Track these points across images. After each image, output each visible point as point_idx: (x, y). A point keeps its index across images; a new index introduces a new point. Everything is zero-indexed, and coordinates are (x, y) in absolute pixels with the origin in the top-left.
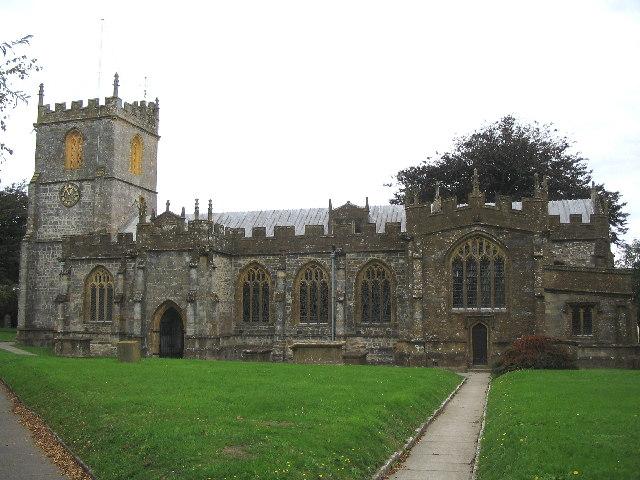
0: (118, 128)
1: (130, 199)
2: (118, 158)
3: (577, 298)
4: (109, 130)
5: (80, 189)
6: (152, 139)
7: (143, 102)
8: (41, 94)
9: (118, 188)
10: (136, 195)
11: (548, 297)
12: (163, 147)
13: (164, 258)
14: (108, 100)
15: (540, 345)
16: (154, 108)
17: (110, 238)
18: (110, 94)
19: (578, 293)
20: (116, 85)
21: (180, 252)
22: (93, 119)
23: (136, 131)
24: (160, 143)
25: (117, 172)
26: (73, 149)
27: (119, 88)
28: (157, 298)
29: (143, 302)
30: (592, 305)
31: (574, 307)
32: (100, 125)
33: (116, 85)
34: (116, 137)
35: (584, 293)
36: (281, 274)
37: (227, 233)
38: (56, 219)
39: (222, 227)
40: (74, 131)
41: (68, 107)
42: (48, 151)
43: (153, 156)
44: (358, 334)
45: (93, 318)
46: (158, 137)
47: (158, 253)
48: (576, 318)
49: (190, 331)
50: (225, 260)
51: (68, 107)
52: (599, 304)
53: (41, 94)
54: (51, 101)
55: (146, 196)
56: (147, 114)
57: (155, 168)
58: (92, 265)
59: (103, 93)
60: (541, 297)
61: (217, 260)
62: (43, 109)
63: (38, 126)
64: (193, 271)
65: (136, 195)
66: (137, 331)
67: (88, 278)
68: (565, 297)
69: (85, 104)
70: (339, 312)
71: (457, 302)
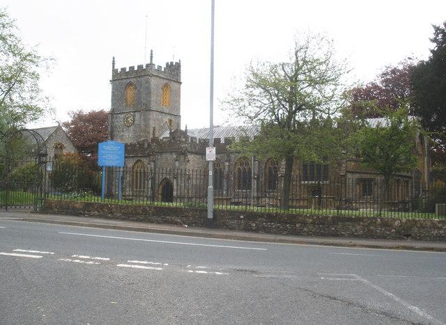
0: (153, 81)
1: (162, 121)
2: (153, 98)
3: (365, 176)
4: (148, 82)
5: (134, 116)
6: (176, 85)
7: (172, 63)
8: (114, 64)
9: (153, 115)
10: (166, 119)
11: (349, 175)
12: (183, 88)
13: (164, 155)
14: (147, 66)
15: (74, 208)
16: (178, 66)
17: (331, 124)
18: (149, 62)
19: (364, 173)
20: (151, 57)
21: (171, 152)
22: (139, 77)
23: (165, 81)
24: (182, 86)
25: (153, 106)
26: (130, 93)
27: (153, 58)
28: (159, 178)
29: (153, 179)
30: (372, 180)
31: (361, 181)
32: (143, 80)
33: (151, 57)
34: (152, 86)
35: (367, 173)
36: (227, 164)
37: (200, 141)
38: (122, 134)
39: (196, 139)
40: (130, 84)
41: (127, 70)
42: (117, 97)
43: (177, 94)
44: (265, 196)
45: (137, 188)
46: (181, 83)
47: (161, 153)
48: (364, 186)
49: (175, 193)
50: (198, 156)
51: (127, 70)
52: (374, 179)
53: (114, 64)
54: (119, 67)
55: (173, 118)
56: (174, 70)
57: (179, 102)
58: (135, 159)
59: (144, 62)
60: (345, 176)
61: (190, 157)
62: (115, 71)
63: (113, 81)
64: (177, 162)
65: (166, 119)
66: (427, 189)
67: (133, 166)
68: (357, 176)
69: (136, 69)
70: (254, 183)
71: (306, 179)
